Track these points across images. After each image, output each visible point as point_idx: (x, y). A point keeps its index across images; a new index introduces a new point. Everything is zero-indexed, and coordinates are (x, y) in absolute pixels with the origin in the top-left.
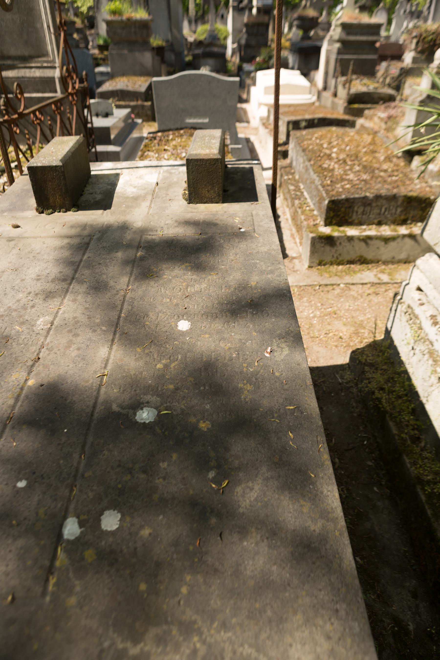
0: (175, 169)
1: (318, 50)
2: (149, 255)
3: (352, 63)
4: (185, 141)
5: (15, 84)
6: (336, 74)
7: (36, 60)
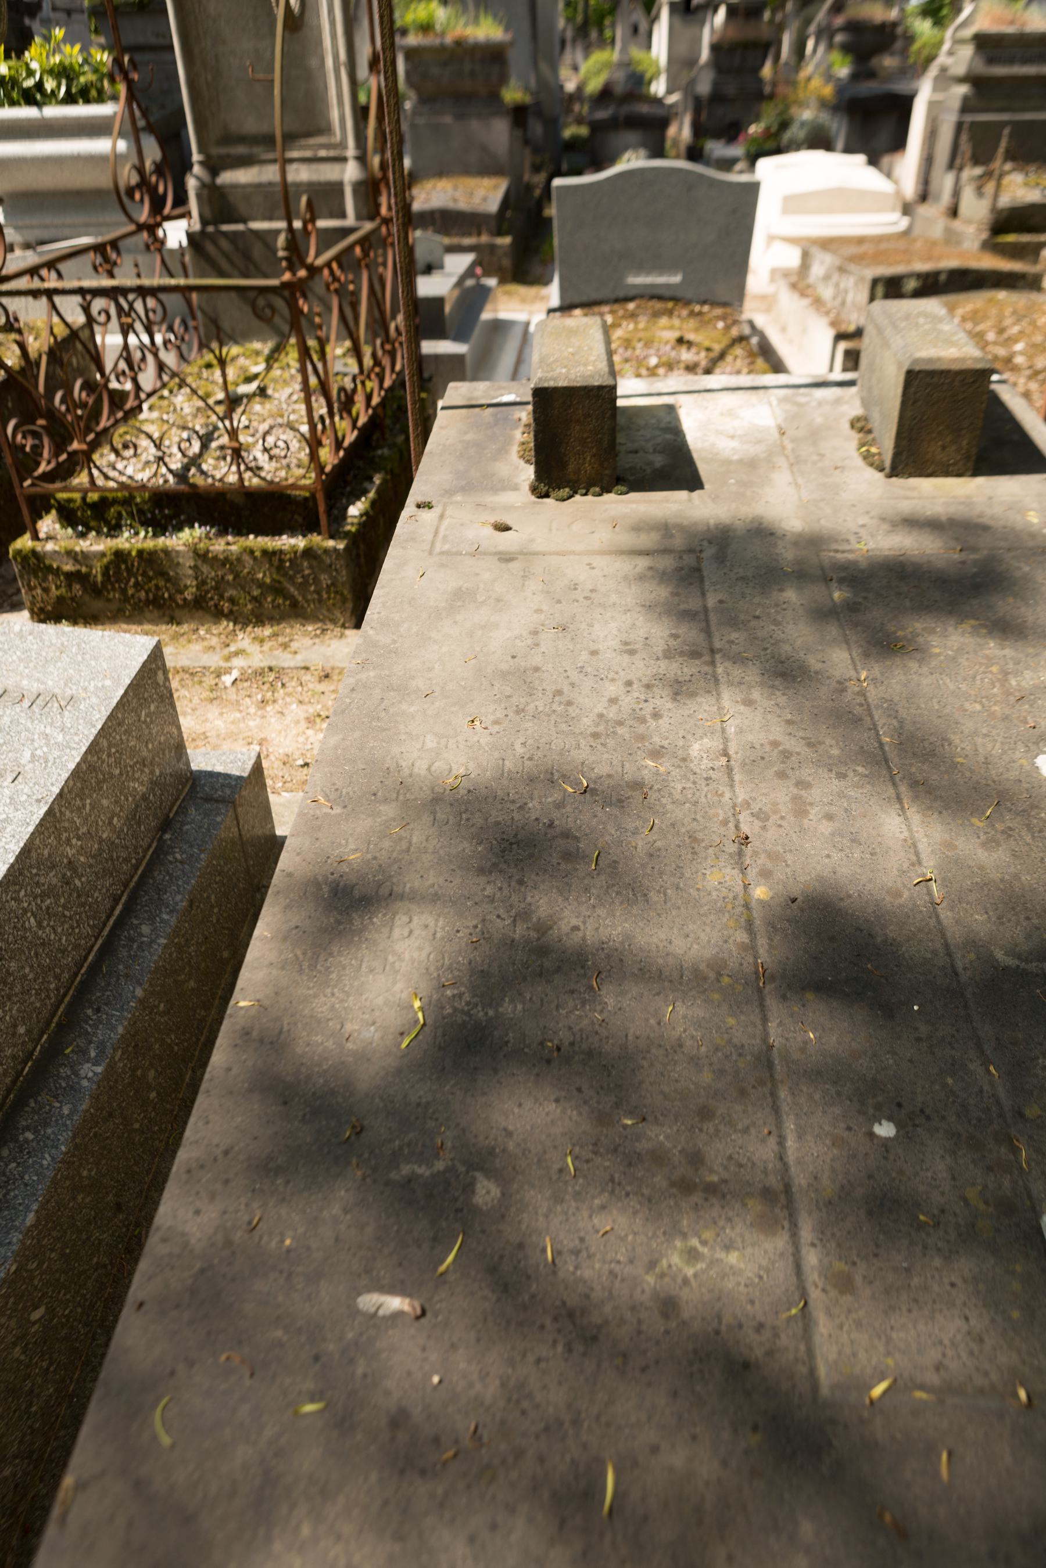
0: (803, 395)
1: (903, 106)
2: (865, 598)
3: (1006, 131)
4: (645, 329)
5: (304, 200)
6: (958, 162)
7: (303, 142)
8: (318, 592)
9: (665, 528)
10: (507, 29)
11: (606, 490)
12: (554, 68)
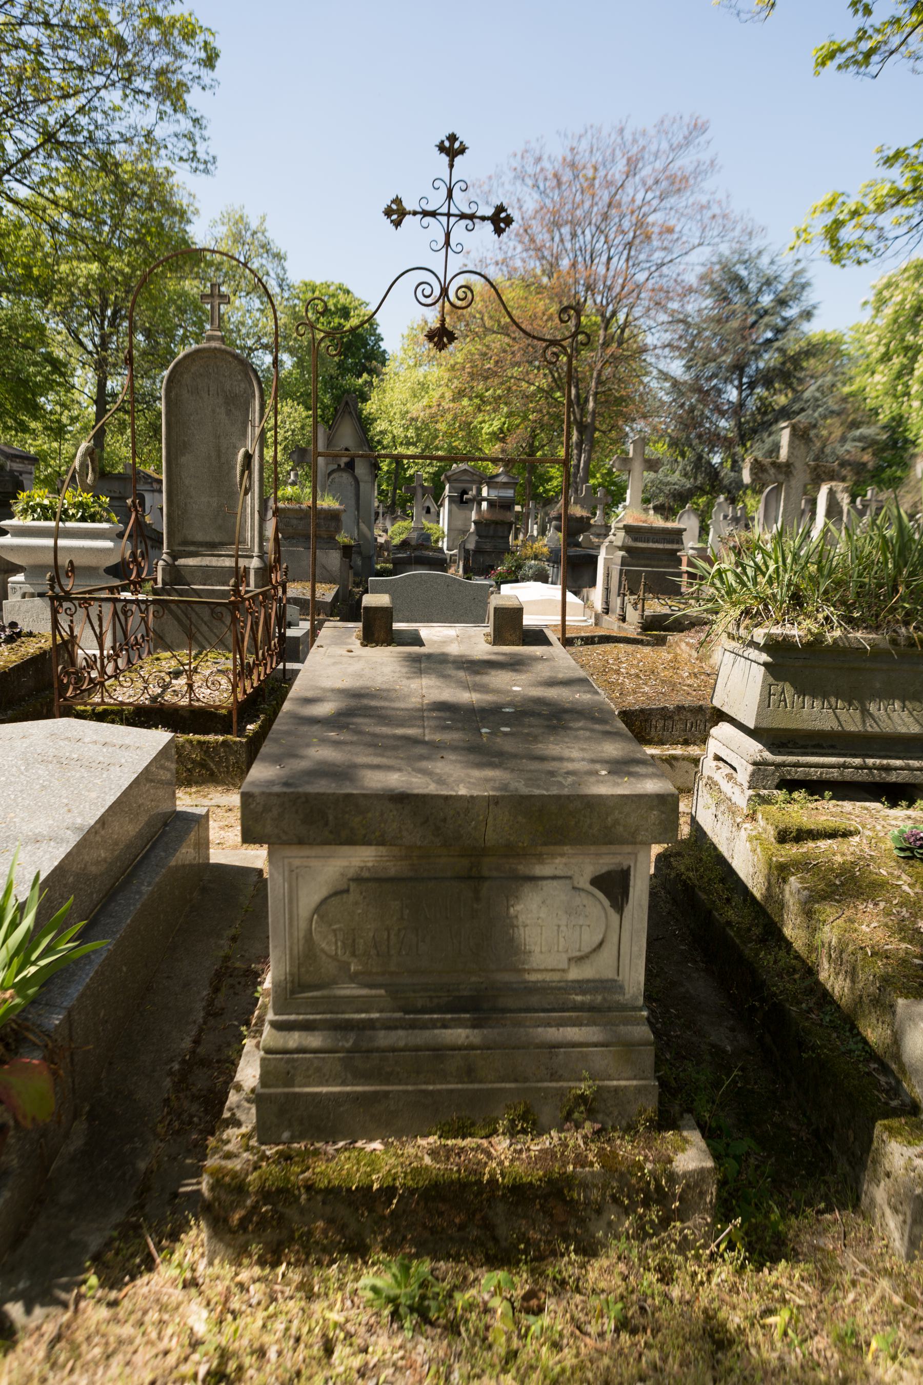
1: (593, 561)
8: (227, 767)
9: (410, 654)
10: (341, 504)
11: (389, 645)
12: (371, 530)
